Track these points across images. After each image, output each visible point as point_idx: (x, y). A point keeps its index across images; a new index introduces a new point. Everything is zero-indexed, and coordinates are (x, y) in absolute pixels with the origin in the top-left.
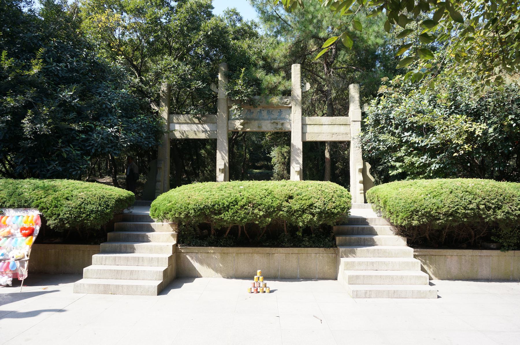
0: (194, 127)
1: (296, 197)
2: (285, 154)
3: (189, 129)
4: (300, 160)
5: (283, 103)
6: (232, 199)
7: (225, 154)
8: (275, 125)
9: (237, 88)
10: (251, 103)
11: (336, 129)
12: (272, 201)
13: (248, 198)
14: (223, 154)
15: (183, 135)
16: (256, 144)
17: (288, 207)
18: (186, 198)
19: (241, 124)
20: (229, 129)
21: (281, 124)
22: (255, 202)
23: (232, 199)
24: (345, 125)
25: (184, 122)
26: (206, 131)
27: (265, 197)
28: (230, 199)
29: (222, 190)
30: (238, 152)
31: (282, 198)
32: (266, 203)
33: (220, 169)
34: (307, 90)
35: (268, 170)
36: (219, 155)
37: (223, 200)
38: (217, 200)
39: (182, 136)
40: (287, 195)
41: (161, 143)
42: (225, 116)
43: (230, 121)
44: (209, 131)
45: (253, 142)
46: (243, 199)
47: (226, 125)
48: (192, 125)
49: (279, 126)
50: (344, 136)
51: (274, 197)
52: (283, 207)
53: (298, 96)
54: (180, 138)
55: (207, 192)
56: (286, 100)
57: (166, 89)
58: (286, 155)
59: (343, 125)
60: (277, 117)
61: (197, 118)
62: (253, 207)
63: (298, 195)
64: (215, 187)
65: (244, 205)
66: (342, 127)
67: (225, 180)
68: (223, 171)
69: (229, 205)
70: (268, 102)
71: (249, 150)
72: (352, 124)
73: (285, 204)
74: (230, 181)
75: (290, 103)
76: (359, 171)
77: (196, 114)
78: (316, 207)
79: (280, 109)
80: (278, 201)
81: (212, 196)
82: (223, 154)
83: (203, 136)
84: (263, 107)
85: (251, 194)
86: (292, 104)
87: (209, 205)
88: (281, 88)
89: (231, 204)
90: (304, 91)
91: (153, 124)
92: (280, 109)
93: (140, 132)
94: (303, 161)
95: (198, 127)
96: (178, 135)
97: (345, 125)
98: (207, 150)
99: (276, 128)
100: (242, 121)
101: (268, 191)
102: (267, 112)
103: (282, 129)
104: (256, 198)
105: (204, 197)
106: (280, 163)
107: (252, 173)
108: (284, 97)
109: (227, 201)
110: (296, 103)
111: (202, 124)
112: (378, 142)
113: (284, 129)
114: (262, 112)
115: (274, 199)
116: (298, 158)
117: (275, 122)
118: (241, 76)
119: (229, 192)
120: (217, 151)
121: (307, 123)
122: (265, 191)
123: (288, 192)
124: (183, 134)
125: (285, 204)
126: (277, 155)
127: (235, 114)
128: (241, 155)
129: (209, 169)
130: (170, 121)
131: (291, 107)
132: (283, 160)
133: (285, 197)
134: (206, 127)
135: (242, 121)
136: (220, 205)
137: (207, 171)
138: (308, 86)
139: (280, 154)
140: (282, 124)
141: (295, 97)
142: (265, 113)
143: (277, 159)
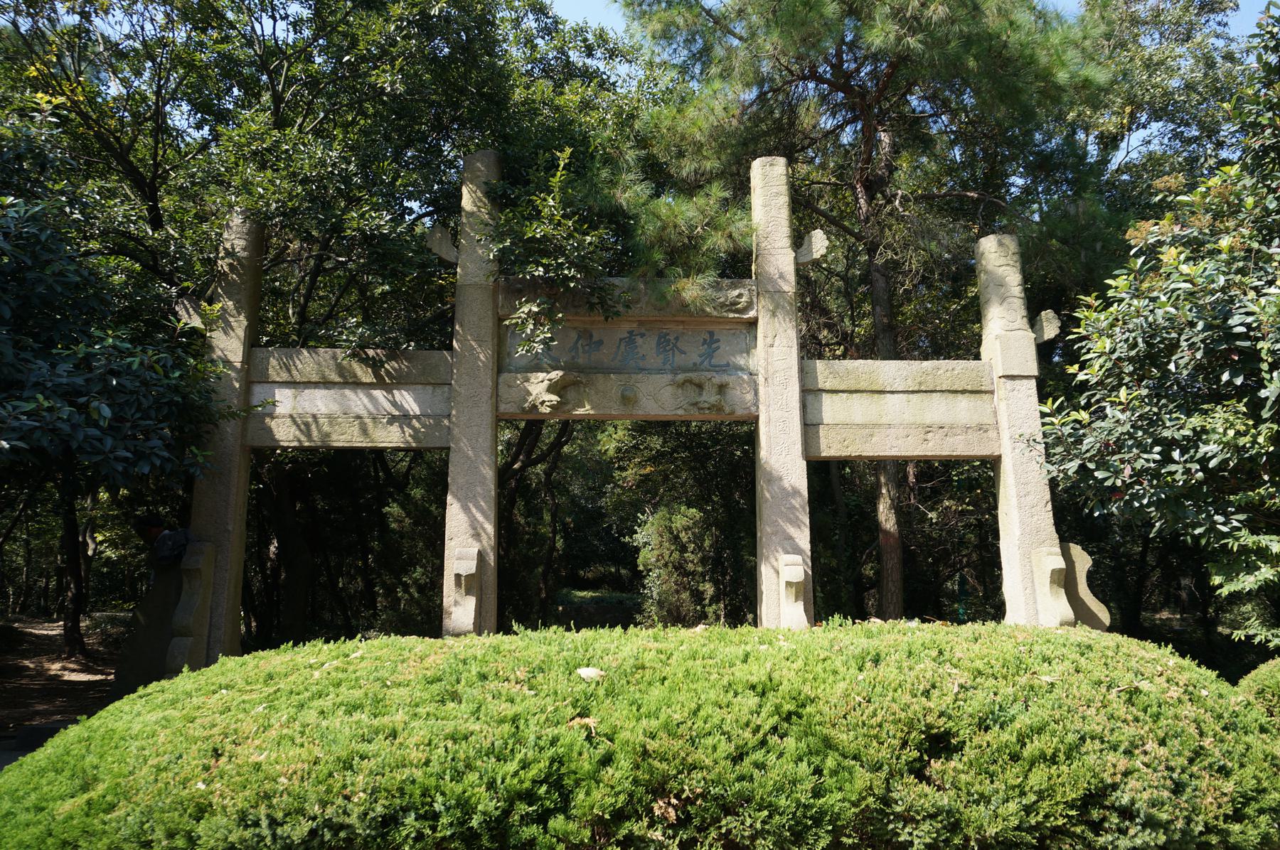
0: (358, 402)
1: (976, 744)
2: (684, 537)
3: (334, 408)
4: (803, 538)
5: (723, 305)
6: (525, 765)
7: (486, 517)
8: (691, 392)
9: (537, 230)
10: (595, 300)
11: (938, 410)
12: (818, 771)
13: (645, 753)
14: (474, 510)
15: (309, 436)
16: (583, 510)
17: (932, 816)
18: (193, 761)
19: (550, 390)
20: (503, 407)
21: (715, 390)
22: (693, 784)
23: (525, 765)
24: (972, 392)
25: (315, 378)
26: (403, 418)
27: (763, 743)
28: (512, 766)
29: (455, 697)
30: (528, 524)
31: (884, 753)
32: (779, 789)
33: (458, 576)
34: (817, 255)
35: (622, 591)
36: (456, 518)
37: (458, 776)
38: (418, 774)
39: (303, 438)
40: (911, 725)
41: (200, 459)
42: (483, 356)
43: (505, 377)
44: (417, 417)
45: (573, 500)
46: (607, 760)
47: (487, 390)
48: (348, 392)
49: (710, 397)
50: (973, 436)
51: (828, 744)
52: (898, 817)
53: (782, 276)
54: (295, 444)
55: (353, 708)
56: (736, 292)
57: (242, 243)
58: (685, 540)
59: (963, 392)
60: (698, 360)
61: (366, 361)
62: (684, 822)
63: (983, 726)
64: (409, 672)
65: (620, 816)
66: (963, 402)
67: (479, 629)
68: (469, 584)
69: (507, 813)
70: (663, 296)
71: (565, 525)
72: (1003, 388)
73: (909, 793)
74: (508, 631)
75: (749, 306)
76: (1053, 582)
77: (363, 345)
78: (1127, 813)
79: (711, 328)
80: (862, 778)
81: (380, 745)
82: (474, 510)
83: (390, 437)
84: (641, 323)
85: (666, 726)
86: (760, 311)
87: (353, 820)
88: (718, 242)
89: (522, 808)
90: (802, 260)
91: (167, 377)
92: (711, 328)
93: (83, 400)
94: (812, 542)
95: (373, 400)
96: (285, 434)
97: (972, 392)
98: (406, 502)
99: (696, 404)
100: (556, 375)
101: (772, 699)
102: (658, 344)
103: (718, 408)
104: (699, 756)
105: (318, 752)
106: (666, 565)
107: (568, 603)
108: (726, 282)
109: (491, 785)
110: (777, 306)
111: (388, 388)
112: (1157, 449)
113: (727, 410)
114: (639, 340)
115: (830, 763)
116: (792, 531)
117: (690, 381)
118: (557, 180)
119: (509, 710)
120: (449, 498)
121: (821, 386)
122: (753, 701)
123: (917, 705)
124: (306, 429)
125: (909, 793)
126: (655, 541)
127: (530, 339)
128: (538, 539)
129: (416, 581)
130: (253, 373)
131: (753, 323)
132: (676, 555)
133: (904, 744)
134: (408, 400)
135: (556, 375)
136: (436, 816)
137: (406, 590)
138: (819, 242)
139: (667, 536)
140: (722, 388)
141: (771, 280)
142: (647, 346)
143: (656, 552)
